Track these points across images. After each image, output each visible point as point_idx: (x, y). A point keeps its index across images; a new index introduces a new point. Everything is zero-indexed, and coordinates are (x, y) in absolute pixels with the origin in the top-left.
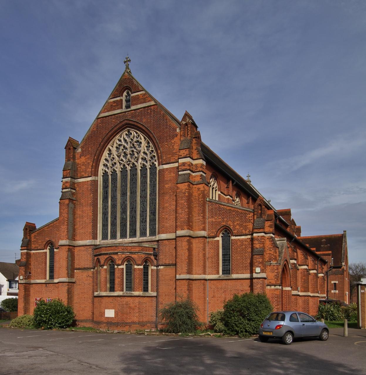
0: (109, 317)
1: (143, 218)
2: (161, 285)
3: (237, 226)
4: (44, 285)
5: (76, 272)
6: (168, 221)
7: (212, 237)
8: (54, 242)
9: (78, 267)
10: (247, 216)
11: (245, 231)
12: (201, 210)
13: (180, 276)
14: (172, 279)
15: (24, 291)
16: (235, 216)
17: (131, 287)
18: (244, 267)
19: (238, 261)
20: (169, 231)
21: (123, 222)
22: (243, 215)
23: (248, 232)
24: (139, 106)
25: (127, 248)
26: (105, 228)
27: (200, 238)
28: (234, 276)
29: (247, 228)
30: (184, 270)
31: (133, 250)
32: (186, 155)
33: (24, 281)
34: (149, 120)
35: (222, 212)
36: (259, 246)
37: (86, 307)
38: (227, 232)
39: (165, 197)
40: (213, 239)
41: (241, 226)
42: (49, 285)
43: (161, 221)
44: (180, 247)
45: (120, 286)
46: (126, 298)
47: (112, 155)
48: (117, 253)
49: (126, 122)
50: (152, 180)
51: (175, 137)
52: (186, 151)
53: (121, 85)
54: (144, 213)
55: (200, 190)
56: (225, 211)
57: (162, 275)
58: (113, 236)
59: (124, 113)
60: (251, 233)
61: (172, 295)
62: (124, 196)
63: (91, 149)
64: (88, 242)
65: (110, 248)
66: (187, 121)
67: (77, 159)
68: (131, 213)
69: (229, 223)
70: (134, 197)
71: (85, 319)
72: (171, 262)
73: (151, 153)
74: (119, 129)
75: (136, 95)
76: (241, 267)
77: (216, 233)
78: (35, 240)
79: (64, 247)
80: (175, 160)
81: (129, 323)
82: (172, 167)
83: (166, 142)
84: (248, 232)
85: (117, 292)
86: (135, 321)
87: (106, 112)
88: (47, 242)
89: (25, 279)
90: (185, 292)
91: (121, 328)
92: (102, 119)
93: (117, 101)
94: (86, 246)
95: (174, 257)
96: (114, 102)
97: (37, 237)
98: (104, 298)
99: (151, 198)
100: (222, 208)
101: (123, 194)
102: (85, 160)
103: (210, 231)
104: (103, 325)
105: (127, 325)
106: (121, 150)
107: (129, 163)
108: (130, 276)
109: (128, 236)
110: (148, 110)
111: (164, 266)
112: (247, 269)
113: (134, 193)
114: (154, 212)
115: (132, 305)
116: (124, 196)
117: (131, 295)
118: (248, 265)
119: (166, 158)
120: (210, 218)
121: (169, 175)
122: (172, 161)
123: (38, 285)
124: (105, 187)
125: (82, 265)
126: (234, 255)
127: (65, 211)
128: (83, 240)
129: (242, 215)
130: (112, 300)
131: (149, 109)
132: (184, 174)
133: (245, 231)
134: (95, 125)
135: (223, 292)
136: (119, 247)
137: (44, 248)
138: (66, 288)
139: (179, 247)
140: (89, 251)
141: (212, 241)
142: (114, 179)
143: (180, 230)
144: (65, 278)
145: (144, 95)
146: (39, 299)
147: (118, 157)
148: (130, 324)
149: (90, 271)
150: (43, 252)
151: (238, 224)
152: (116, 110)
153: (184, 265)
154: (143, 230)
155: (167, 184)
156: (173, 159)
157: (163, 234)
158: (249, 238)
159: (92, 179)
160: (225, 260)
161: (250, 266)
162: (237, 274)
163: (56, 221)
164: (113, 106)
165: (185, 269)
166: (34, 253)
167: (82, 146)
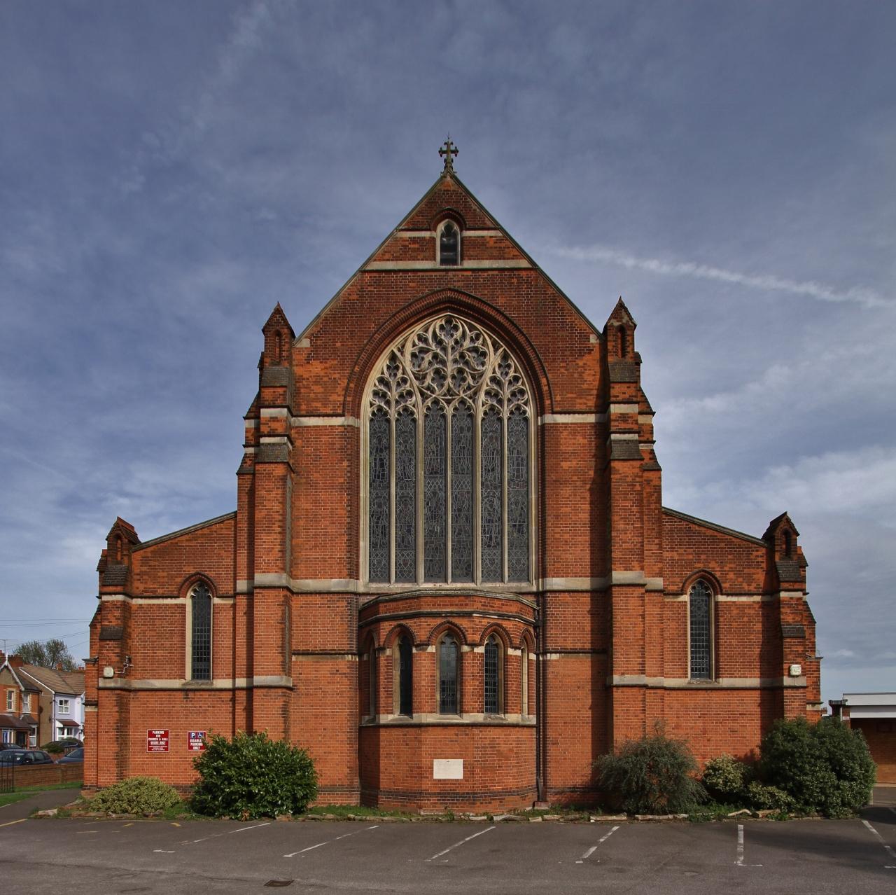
0: (444, 780)
1: (491, 536)
2: (553, 699)
3: (730, 573)
4: (181, 695)
5: (295, 662)
6: (570, 547)
7: (673, 594)
8: (212, 578)
9: (301, 648)
10: (752, 554)
11: (749, 585)
12: (654, 529)
13: (623, 677)
14: (583, 685)
15: (116, 709)
16: (726, 551)
17: (454, 703)
18: (748, 662)
19: (733, 651)
20: (572, 570)
21: (432, 543)
22: (744, 551)
23: (755, 588)
24: (486, 264)
25: (492, 603)
26: (377, 552)
27: (653, 594)
28: (725, 682)
29: (754, 579)
30: (633, 664)
31: (506, 610)
32: (630, 396)
33: (116, 682)
34: (515, 303)
35: (695, 539)
36: (793, 619)
37: (330, 753)
38: (707, 584)
39: (562, 490)
40: (674, 598)
41: (739, 574)
42: (197, 693)
43: (552, 548)
44: (623, 609)
45: (478, 699)
46: (492, 729)
47: (401, 371)
48: (469, 615)
49: (449, 294)
50: (514, 448)
51: (585, 353)
52: (628, 387)
53: (432, 202)
54: (494, 525)
55: (652, 483)
56: (702, 539)
57: (556, 676)
58: (403, 575)
59: (444, 273)
60: (761, 590)
61: (583, 723)
62: (433, 477)
63: (343, 345)
64: (334, 584)
65: (447, 599)
66: (624, 321)
67: (297, 365)
68: (457, 521)
69: (711, 565)
70: (464, 483)
71: (327, 785)
72: (579, 646)
73: (399, 384)
74: (427, 307)
75: (478, 237)
76: (741, 662)
77: (681, 585)
78: (144, 569)
79: (273, 593)
80: (587, 407)
81: (499, 792)
82: (580, 423)
83: (562, 362)
84: (755, 588)
85: (471, 714)
86: (511, 788)
87: (388, 260)
88: (190, 577)
89: (120, 676)
90: (636, 716)
91: (481, 805)
92: (375, 274)
93: (423, 239)
94: (329, 593)
95: (587, 634)
96: (414, 240)
97: (152, 563)
98: (430, 729)
99: (511, 489)
100: (696, 530)
101: (431, 473)
102: (324, 371)
103: (668, 579)
104: (429, 800)
105: (496, 799)
106: (425, 364)
107: (449, 397)
108: (493, 675)
109: (450, 580)
110: (513, 278)
111: (560, 653)
112: (753, 668)
113: (463, 474)
114: (520, 525)
115: (504, 748)
116: (433, 477)
117: (501, 722)
118: (755, 659)
119: (563, 400)
120: (668, 551)
121: (571, 439)
122: (578, 407)
123: (158, 693)
124: (380, 448)
125: (317, 643)
126: (725, 636)
127: (273, 494)
128: (319, 578)
129: (739, 551)
130: (457, 735)
131: (514, 275)
132: (625, 440)
133: (748, 585)
134: (357, 286)
135: (700, 717)
136: (476, 599)
137: (179, 593)
138: (280, 702)
139: (620, 609)
140: (338, 607)
141: (672, 602)
142: (405, 432)
143: (621, 570)
144: (274, 676)
145: (499, 240)
146: (163, 733)
147: (417, 378)
148: (501, 796)
149: (342, 658)
150: (176, 605)
151: (731, 570)
152: (418, 260)
153: (633, 652)
154: (492, 564)
155: (566, 460)
156: (581, 404)
157: (557, 577)
158: (758, 602)
159: (346, 424)
160: (198, 655)
161: (761, 662)
162: (730, 677)
163: (221, 523)
164: (410, 248)
165: (636, 661)
166: (141, 605)
167: (313, 334)
